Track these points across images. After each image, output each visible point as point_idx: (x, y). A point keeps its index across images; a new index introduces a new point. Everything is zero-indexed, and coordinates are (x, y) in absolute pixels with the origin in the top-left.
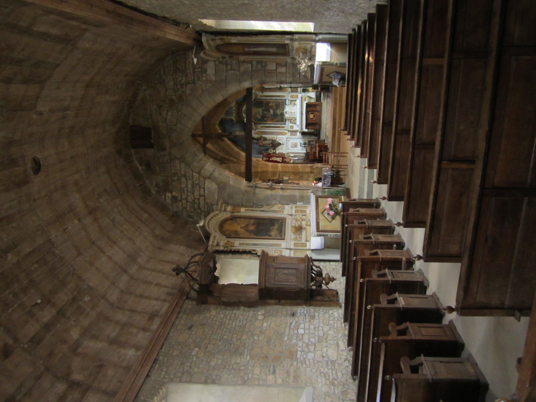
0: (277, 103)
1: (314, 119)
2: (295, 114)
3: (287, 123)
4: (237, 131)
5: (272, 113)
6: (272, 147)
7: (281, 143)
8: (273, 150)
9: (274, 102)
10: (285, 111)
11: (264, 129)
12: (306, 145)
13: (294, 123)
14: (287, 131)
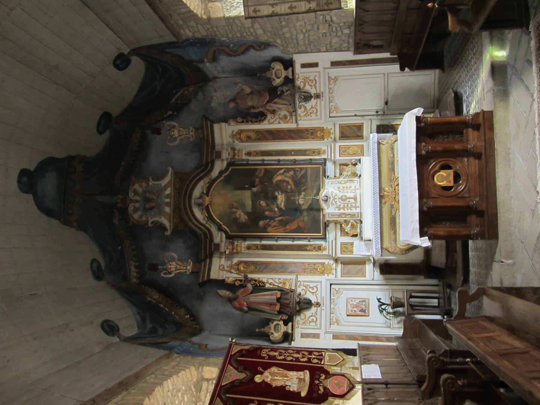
0: (300, 175)
1: (461, 188)
2: (358, 205)
3: (331, 235)
4: (173, 260)
5: (282, 206)
6: (280, 312)
7: (314, 300)
8: (286, 323)
9: (287, 170)
10: (323, 193)
11: (260, 256)
12: (401, 309)
13: (356, 236)
14: (332, 262)
